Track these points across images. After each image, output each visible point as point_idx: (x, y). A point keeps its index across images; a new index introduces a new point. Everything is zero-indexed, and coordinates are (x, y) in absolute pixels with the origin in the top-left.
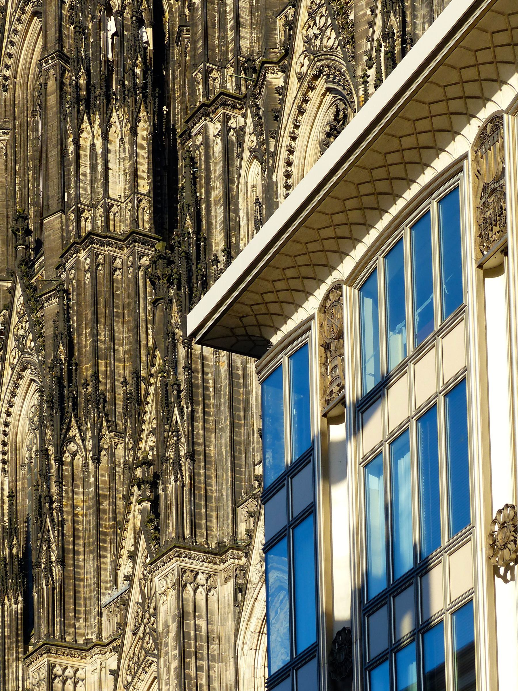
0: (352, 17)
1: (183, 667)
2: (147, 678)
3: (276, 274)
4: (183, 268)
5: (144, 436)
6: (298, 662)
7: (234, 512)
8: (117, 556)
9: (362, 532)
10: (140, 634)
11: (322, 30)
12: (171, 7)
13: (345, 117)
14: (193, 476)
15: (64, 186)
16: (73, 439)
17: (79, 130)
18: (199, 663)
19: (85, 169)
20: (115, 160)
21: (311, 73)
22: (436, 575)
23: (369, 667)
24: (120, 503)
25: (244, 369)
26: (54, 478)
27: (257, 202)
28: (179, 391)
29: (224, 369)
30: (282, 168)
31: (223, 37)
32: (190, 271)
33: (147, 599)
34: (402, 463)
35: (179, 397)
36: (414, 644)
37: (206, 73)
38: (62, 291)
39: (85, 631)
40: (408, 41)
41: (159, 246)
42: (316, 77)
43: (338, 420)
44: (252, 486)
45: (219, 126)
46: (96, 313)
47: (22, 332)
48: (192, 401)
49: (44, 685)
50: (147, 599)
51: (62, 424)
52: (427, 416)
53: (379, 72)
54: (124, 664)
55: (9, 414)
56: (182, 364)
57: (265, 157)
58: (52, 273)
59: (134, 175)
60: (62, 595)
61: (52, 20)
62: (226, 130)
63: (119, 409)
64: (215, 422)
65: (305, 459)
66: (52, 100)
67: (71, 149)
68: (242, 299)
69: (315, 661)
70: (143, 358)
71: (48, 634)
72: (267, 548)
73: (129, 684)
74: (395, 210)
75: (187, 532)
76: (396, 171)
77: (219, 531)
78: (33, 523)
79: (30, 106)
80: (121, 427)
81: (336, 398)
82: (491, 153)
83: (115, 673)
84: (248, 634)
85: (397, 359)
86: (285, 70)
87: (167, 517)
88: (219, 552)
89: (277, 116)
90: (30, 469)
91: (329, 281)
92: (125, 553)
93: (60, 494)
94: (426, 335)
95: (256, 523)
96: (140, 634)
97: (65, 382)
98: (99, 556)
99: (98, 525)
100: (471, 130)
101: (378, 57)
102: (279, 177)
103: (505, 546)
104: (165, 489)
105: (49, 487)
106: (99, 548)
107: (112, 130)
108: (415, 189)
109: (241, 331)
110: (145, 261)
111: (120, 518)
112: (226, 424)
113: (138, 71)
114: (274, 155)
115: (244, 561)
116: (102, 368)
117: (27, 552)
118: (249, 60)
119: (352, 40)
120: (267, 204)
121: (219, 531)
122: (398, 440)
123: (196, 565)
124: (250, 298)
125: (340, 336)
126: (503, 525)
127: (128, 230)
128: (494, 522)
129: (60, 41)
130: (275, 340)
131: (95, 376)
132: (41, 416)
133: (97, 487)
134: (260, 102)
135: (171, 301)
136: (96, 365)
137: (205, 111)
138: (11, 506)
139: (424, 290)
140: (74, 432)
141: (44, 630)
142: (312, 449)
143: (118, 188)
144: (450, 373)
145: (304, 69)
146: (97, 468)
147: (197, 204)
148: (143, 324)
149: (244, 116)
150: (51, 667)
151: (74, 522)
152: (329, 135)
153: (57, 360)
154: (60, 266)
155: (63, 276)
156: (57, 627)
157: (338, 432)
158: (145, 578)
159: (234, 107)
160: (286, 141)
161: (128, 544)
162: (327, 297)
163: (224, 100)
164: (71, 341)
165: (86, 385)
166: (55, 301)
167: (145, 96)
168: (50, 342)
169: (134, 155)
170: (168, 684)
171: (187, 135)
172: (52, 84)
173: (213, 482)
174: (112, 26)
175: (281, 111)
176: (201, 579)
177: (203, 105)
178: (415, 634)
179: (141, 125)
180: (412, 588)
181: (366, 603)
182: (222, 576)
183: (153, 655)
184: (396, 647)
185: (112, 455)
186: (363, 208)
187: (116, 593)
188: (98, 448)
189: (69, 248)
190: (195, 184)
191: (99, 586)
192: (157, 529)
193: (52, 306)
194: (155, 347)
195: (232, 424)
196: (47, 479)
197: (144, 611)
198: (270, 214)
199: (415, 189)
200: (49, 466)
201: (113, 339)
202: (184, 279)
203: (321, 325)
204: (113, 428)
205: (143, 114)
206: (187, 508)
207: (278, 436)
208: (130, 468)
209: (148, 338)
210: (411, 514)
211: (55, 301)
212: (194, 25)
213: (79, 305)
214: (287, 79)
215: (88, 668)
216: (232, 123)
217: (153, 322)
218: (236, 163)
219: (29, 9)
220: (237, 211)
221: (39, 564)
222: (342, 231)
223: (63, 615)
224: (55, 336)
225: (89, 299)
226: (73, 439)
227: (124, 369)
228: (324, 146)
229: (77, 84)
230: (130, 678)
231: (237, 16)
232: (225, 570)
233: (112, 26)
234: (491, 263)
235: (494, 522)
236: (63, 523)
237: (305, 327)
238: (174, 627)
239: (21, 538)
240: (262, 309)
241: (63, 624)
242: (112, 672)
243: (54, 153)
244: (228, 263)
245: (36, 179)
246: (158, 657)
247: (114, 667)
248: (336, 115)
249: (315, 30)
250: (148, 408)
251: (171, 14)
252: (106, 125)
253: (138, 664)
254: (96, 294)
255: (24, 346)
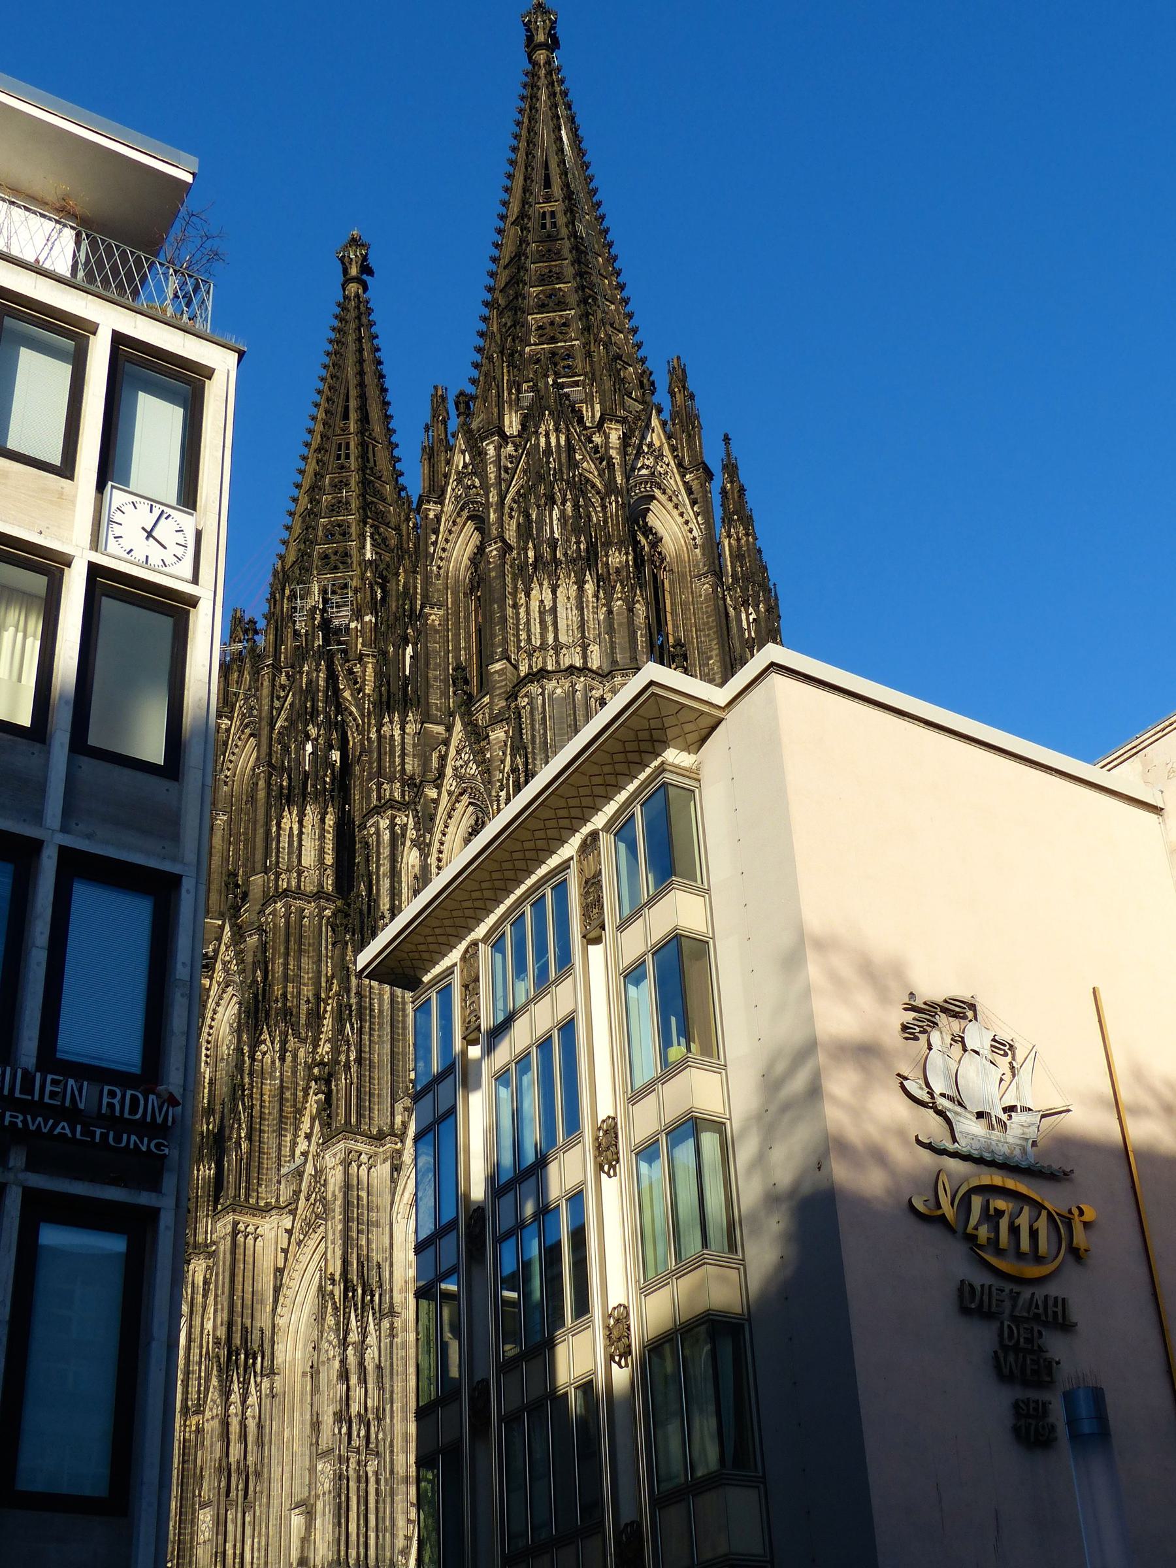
0: (488, 756)
1: (346, 1230)
2: (316, 1237)
3: (428, 931)
4: (358, 922)
5: (321, 1043)
6: (441, 1232)
7: (393, 1107)
8: (296, 1136)
9: (493, 1132)
10: (312, 1200)
11: (467, 763)
12: (354, 738)
13: (483, 823)
14: (359, 1078)
15: (267, 855)
16: (264, 1042)
17: (280, 818)
18: (360, 1227)
19: (285, 843)
20: (308, 840)
21: (457, 791)
22: (553, 1169)
23: (500, 1240)
24: (300, 1094)
25: (403, 997)
26: (247, 1072)
27: (416, 877)
28: (351, 1011)
29: (387, 996)
30: (435, 855)
31: (392, 762)
32: (362, 922)
33: (319, 1172)
34: (525, 1079)
35: (350, 1015)
36: (536, 1223)
37: (379, 785)
38: (261, 930)
39: (266, 1196)
40: (530, 775)
41: (339, 903)
42: (461, 794)
43: (474, 1042)
44: (407, 1087)
45: (388, 822)
46: (287, 948)
47: (228, 958)
48: (360, 1017)
49: (229, 1238)
50: (319, 1172)
51: (256, 1030)
52: (544, 1044)
53: (508, 793)
54: (297, 1225)
55: (213, 1019)
56: (354, 990)
57: (423, 847)
58: (254, 917)
59: (321, 851)
60: (248, 1164)
61: (264, 740)
62: (392, 825)
63: (303, 1021)
64: (379, 1036)
65: (448, 1070)
66: (261, 795)
67: (274, 829)
68: (640, 712)
69: (455, 1232)
70: (323, 984)
71: (235, 1197)
72: (417, 1139)
73: (301, 1241)
74: (519, 892)
75: (353, 1120)
76: (520, 865)
77: (380, 1121)
78: (228, 1105)
79: (244, 797)
80: (303, 1035)
81: (473, 1026)
82: (591, 858)
83: (289, 1232)
84: (402, 1206)
85: (521, 1000)
86: (439, 787)
87: (337, 1108)
88: (380, 1137)
89: (432, 818)
90: (228, 1063)
91: (469, 939)
92: (302, 1134)
93: (251, 1084)
94: (543, 983)
95: (409, 1117)
96: (312, 1200)
97: (260, 998)
98: (280, 1135)
99: (281, 1110)
100: (576, 841)
101: (508, 783)
102: (432, 860)
103: (608, 1148)
104: (336, 1085)
105: (242, 1078)
106: (281, 1129)
107: (306, 818)
108: (533, 879)
109: (400, 971)
110: (328, 913)
111: (299, 1106)
112: (387, 1038)
113: (328, 780)
114: (429, 845)
115: (399, 1145)
116: (290, 989)
117: (222, 1128)
118: (412, 778)
119: (488, 771)
120: (423, 878)
121: (380, 1121)
122: (522, 1061)
123: (360, 1147)
124: (407, 947)
125: (477, 980)
126: (606, 1132)
127: (315, 890)
128: (599, 1129)
129: (270, 755)
130: (426, 979)
131: (284, 995)
132: (239, 1023)
133: (282, 1081)
134: (419, 808)
135: (347, 944)
136: (285, 987)
137: (378, 810)
138: (210, 1091)
139: (541, 950)
140: (265, 1036)
141: (232, 1193)
142: (454, 1063)
143: (309, 858)
144: (562, 1012)
145: (453, 788)
146: (282, 1065)
147: (370, 874)
148: (324, 959)
149: (407, 816)
150: (235, 1224)
151: (261, 1106)
152: (471, 834)
153: (254, 981)
154: (261, 912)
155: (263, 919)
156: (243, 1191)
157: (474, 1052)
158: (318, 1155)
159: (399, 810)
160: (438, 836)
161: (305, 1127)
162: (466, 951)
163: (391, 804)
164: (267, 967)
165: (277, 1001)
166: (256, 937)
167: (332, 797)
168: (249, 967)
169: (322, 837)
170: (333, 1243)
171: (363, 826)
172: (262, 784)
173: (376, 1082)
174: (309, 748)
175: (435, 815)
176: (364, 1158)
177: (376, 806)
178: (536, 1216)
179: (328, 816)
180: (513, 1192)
181: (497, 1187)
182: (382, 1157)
183: (321, 1218)
184: (520, 1225)
185: (295, 1056)
186: (640, 752)
187: (293, 1166)
188: (283, 1050)
189: (268, 900)
190: (368, 861)
191: (279, 1159)
192: (329, 1116)
193: (253, 940)
194: (333, 977)
195: (392, 1038)
196: (241, 1071)
197: (316, 1182)
198: (425, 885)
199: (533, 879)
200: (243, 1062)
201: (300, 968)
202: (357, 928)
203: (462, 971)
204: (297, 1035)
205: (330, 809)
206: (354, 1101)
207: (429, 1050)
208: (309, 1068)
209: (328, 969)
210: (532, 1120)
211: (256, 937)
212: (371, 752)
213: (274, 941)
214: (439, 794)
215: (267, 1226)
216: (398, 821)
217: (332, 958)
218: (400, 848)
219: (248, 731)
220: (400, 882)
221: (231, 1139)
222: (478, 904)
223: (248, 1181)
224: (254, 963)
225: (282, 937)
226: (264, 1042)
227: (307, 991)
228: (467, 841)
229: (281, 785)
230: (302, 1237)
231: (403, 749)
232: (384, 1152)
233: (309, 748)
234: (592, 935)
235: (599, 1129)
236: (252, 1107)
237: (449, 971)
238: (340, 1196)
239: (217, 1117)
240: (417, 956)
241: (247, 1189)
242: (287, 1231)
243: (261, 831)
244: (392, 919)
245: (246, 848)
246: (326, 1220)
247: (289, 1227)
248: (477, 821)
249: (461, 762)
250: (325, 1022)
251: (354, 743)
252: (302, 815)
253: (309, 1225)
254: (288, 935)
255: (229, 969)
